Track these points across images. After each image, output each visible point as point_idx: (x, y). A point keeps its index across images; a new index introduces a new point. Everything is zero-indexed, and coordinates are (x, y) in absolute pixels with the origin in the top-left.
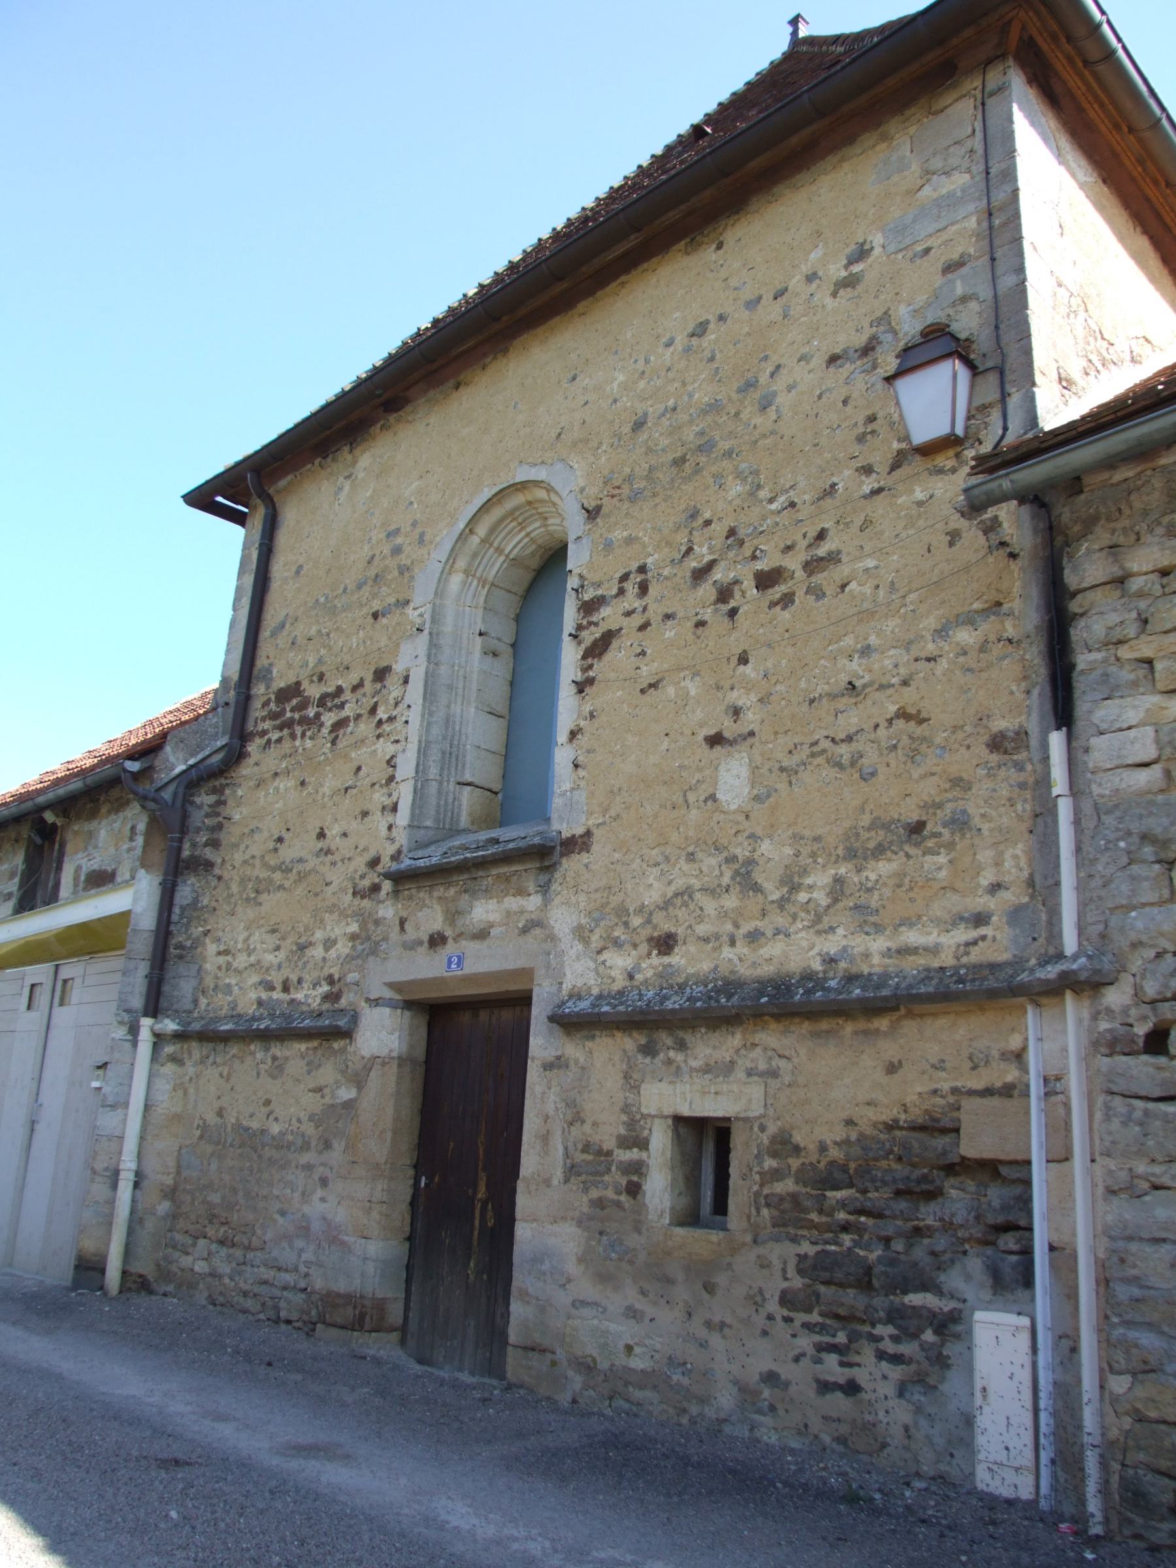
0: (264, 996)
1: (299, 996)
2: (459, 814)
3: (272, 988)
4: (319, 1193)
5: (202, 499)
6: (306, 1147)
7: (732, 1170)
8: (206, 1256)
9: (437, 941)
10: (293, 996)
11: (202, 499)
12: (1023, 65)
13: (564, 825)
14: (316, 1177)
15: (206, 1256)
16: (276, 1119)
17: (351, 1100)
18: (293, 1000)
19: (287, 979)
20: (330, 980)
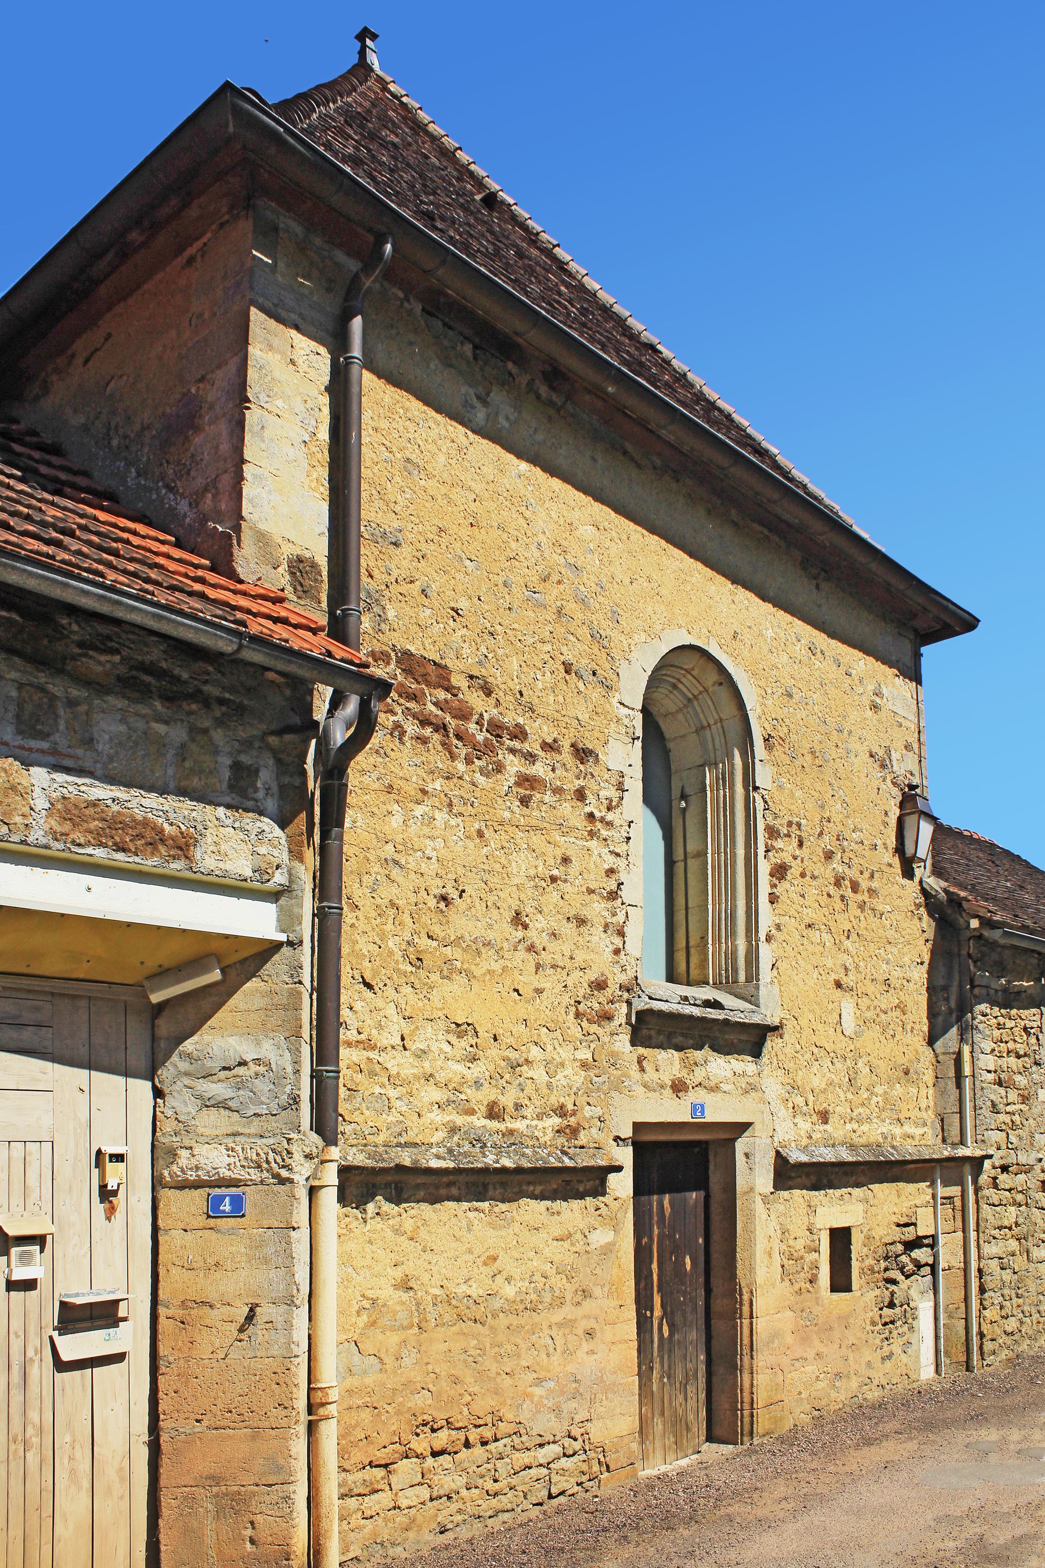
0: (460, 1120)
1: (519, 1125)
2: (736, 950)
3: (471, 1112)
4: (586, 1346)
5: (968, 623)
6: (560, 1301)
7: (852, 1256)
8: (419, 1479)
9: (679, 1087)
10: (510, 1126)
11: (968, 623)
12: (362, 699)
13: (768, 1013)
14: (580, 1331)
15: (419, 1479)
16: (508, 1280)
17: (609, 1244)
18: (511, 1132)
19: (495, 1103)
20: (561, 1111)
